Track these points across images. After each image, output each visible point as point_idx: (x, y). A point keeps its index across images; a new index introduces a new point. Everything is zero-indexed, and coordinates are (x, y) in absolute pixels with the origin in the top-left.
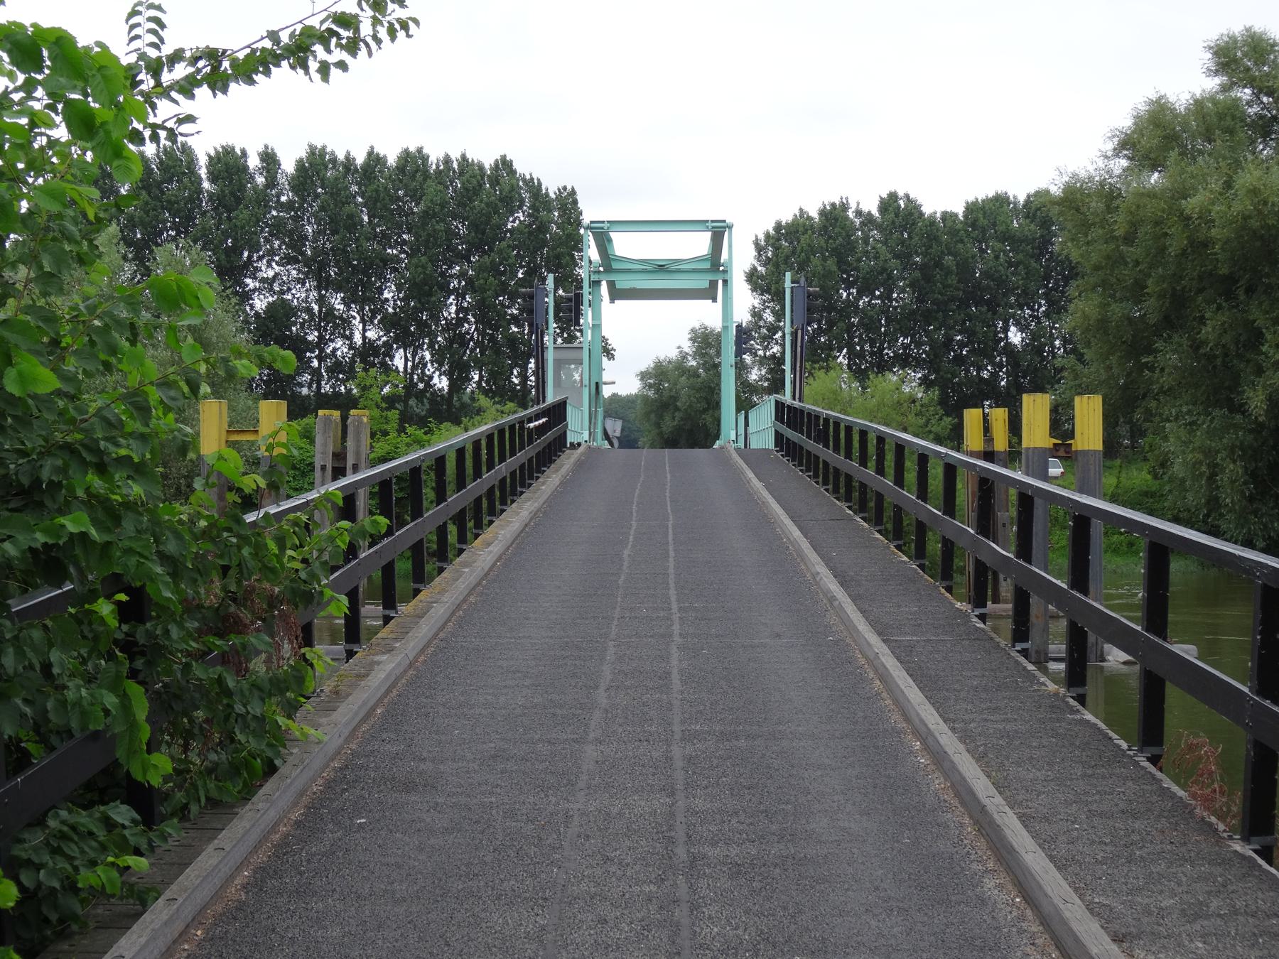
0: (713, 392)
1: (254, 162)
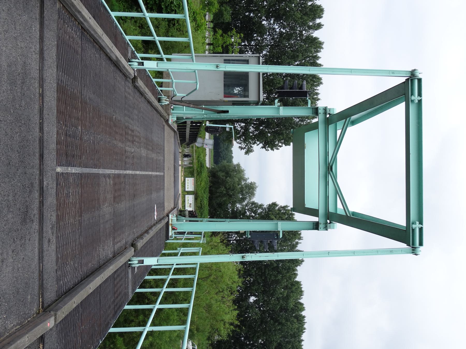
0: (232, 190)
1: (318, 21)
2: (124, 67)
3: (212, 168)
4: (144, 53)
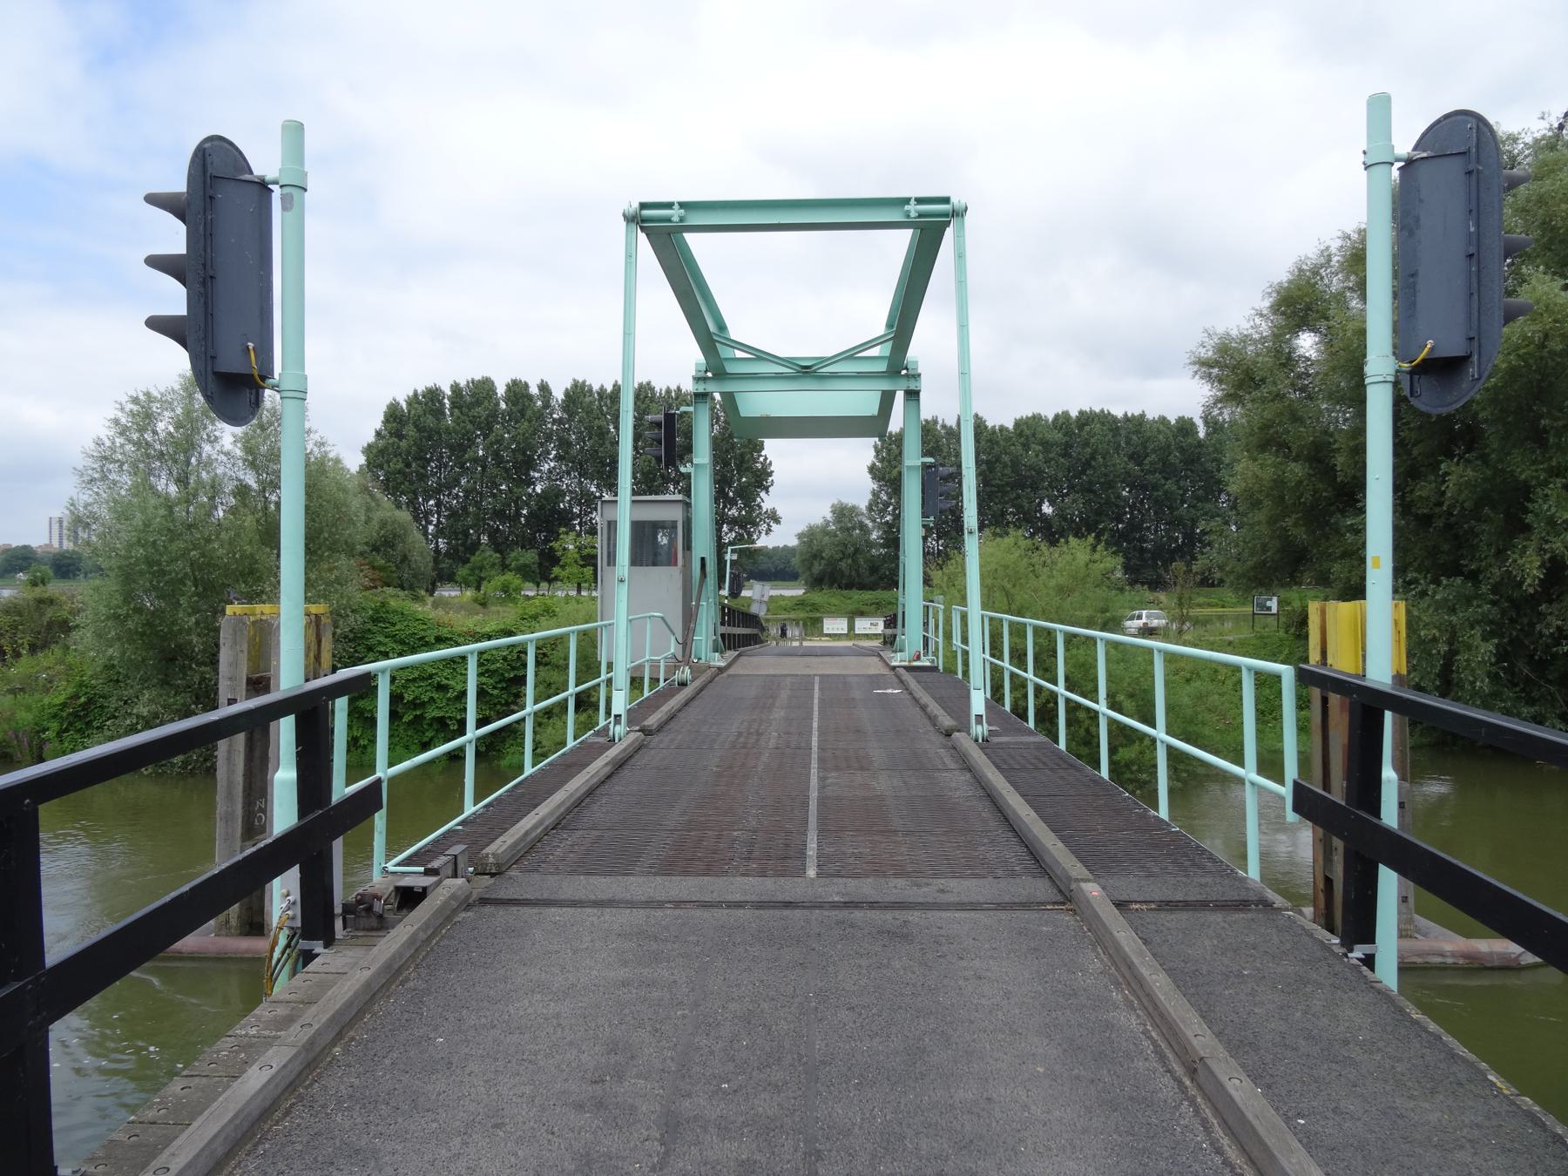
1: (534, 390)
2: (625, 750)
3: (806, 584)
4: (598, 710)
